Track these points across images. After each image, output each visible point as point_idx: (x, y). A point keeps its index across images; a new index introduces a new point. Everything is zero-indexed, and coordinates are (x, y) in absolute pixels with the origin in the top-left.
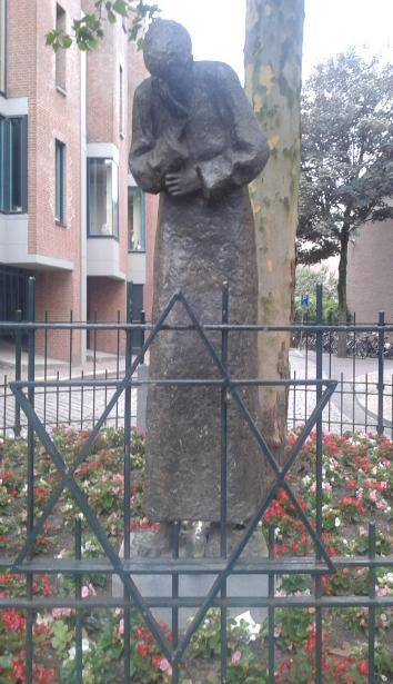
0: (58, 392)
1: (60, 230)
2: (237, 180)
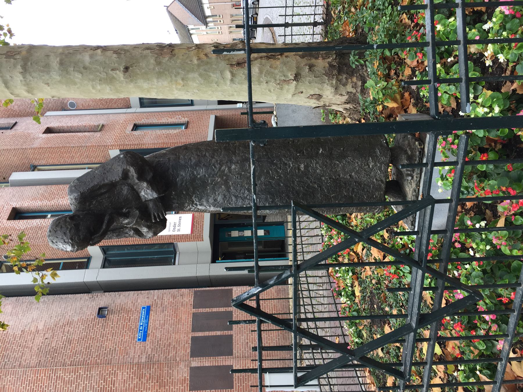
0: (301, 229)
1: (190, 126)
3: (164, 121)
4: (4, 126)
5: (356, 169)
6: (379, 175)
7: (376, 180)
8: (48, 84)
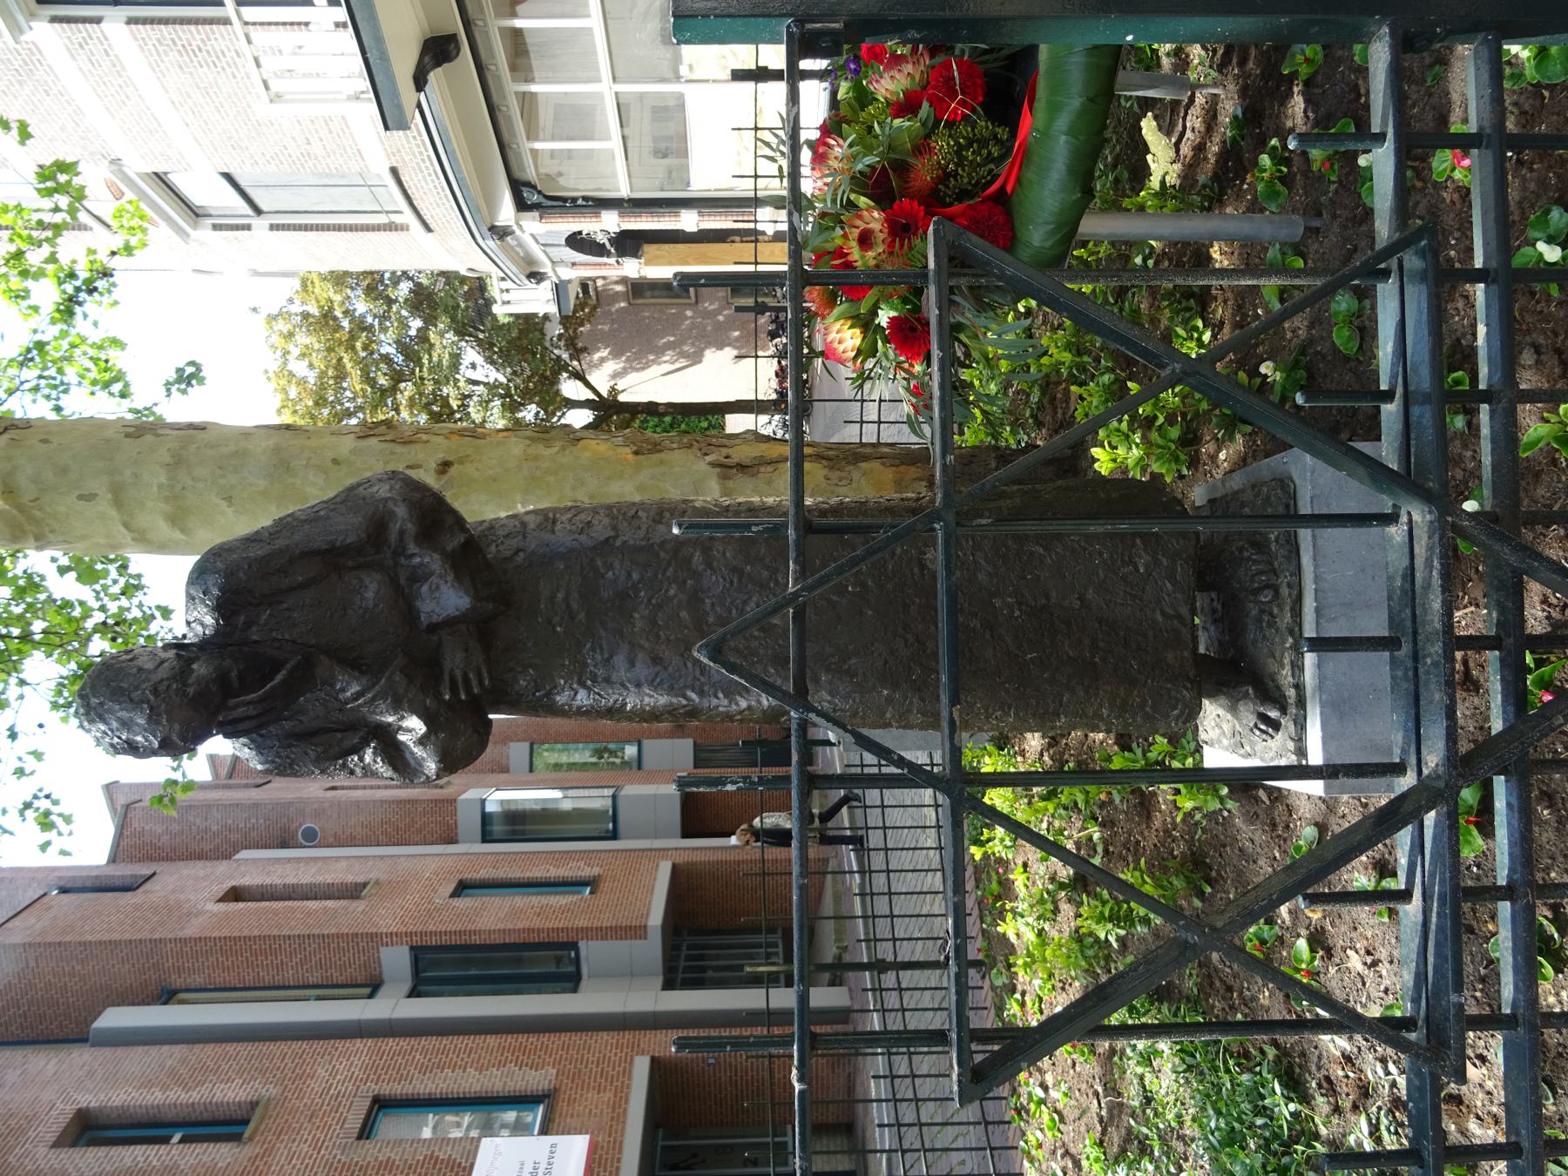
1: (605, 887)
2: (453, 542)
3: (537, 873)
4: (118, 883)
5: (1098, 574)
6: (1169, 595)
7: (1163, 613)
8: (229, 499)
